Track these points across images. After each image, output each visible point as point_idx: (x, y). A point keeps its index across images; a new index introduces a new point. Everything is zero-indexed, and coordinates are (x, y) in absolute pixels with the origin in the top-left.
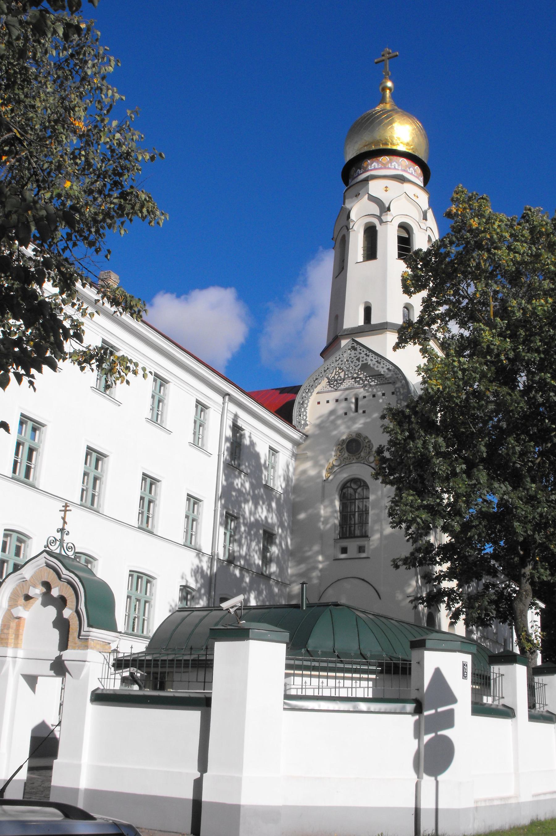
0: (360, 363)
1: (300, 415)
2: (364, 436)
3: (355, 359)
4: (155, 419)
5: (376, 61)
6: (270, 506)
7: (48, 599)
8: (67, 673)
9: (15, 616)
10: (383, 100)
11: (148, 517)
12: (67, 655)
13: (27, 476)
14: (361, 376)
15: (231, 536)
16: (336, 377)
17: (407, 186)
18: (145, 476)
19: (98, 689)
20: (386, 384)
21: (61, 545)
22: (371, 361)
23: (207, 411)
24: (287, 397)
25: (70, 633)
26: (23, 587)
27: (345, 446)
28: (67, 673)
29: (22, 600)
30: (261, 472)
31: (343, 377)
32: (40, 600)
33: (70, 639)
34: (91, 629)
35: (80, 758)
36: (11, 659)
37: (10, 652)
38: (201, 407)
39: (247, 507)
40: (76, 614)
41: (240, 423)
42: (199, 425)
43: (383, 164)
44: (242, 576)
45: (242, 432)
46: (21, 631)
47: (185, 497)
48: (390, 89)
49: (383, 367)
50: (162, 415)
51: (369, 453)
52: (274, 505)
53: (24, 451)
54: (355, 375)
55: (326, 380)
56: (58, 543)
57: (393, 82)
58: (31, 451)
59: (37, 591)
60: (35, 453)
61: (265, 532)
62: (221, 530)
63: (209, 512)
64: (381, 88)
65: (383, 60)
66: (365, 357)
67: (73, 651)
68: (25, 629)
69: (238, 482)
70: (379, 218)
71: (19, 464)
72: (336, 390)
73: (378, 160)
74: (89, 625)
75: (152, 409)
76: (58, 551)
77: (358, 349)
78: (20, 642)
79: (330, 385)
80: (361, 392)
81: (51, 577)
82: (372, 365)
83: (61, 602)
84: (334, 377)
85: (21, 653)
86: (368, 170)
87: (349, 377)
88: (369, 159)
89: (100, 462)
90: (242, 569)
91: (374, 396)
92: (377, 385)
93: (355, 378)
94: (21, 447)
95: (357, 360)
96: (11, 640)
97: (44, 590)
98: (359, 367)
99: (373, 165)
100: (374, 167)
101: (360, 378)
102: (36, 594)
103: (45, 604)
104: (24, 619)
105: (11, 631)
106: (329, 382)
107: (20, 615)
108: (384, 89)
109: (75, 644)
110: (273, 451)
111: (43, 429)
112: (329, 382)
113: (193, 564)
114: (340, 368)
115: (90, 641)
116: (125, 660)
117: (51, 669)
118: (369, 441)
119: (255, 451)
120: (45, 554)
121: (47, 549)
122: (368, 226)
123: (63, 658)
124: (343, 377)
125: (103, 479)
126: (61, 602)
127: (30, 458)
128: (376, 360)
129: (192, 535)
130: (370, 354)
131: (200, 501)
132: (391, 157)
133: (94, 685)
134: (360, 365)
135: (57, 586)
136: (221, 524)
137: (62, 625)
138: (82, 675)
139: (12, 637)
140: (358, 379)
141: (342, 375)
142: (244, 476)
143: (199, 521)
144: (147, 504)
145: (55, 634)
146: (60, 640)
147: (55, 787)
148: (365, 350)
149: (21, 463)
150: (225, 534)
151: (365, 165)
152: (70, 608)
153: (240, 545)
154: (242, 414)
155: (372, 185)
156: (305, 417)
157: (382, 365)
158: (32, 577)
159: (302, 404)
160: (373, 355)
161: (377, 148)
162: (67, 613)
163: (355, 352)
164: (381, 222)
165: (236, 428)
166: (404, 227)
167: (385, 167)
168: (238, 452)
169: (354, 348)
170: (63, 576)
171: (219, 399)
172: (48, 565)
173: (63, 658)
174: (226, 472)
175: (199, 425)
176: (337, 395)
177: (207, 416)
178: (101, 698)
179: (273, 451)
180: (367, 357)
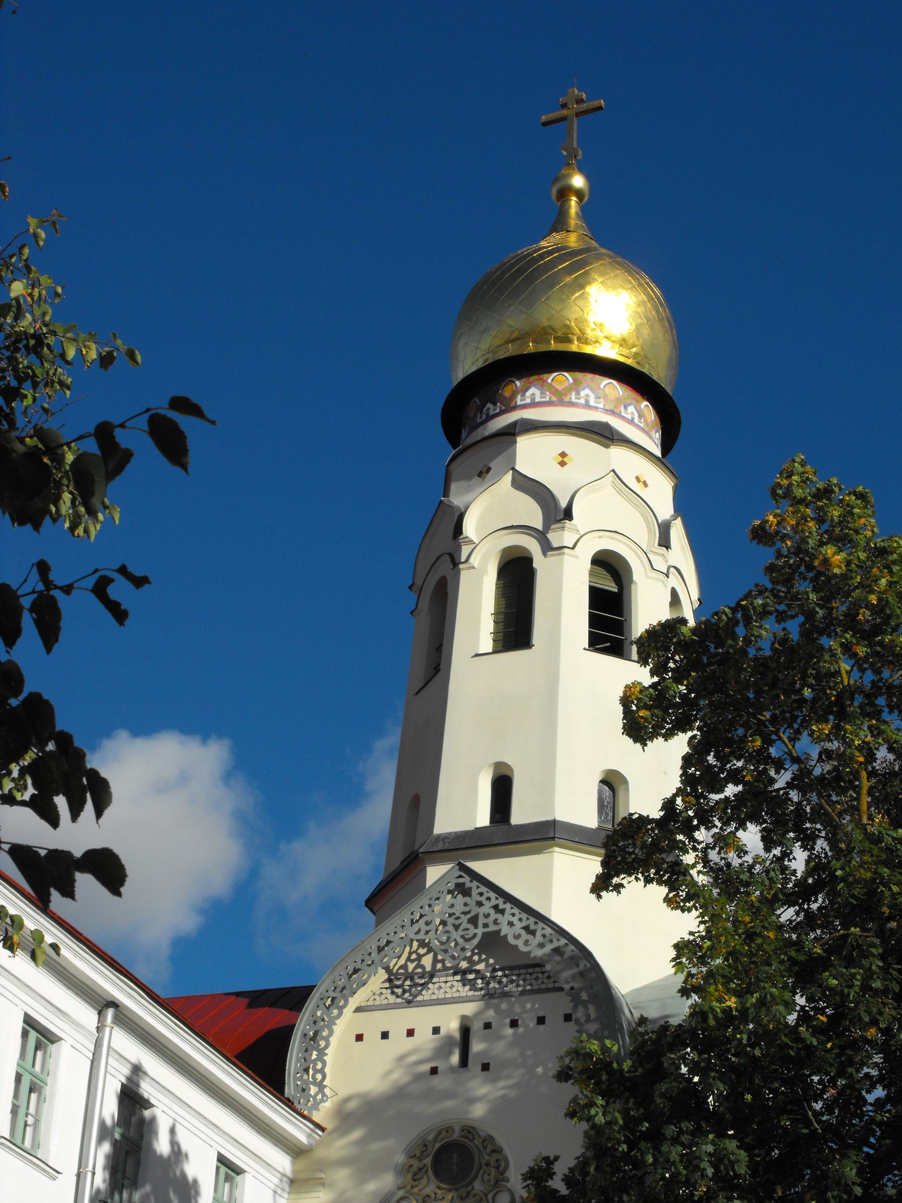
0: (480, 931)
1: (306, 1070)
3: (464, 919)
5: (544, 118)
10: (559, 223)
14: (481, 967)
16: (411, 967)
17: (618, 455)
22: (511, 927)
23: (52, 1048)
24: (269, 1019)
27: (428, 1161)
31: (428, 968)
38: (37, 1036)
41: (146, 1089)
43: (555, 392)
48: (579, 194)
51: (497, 1182)
55: (382, 975)
64: (554, 190)
65: (564, 119)
66: (493, 915)
70: (541, 536)
73: (545, 381)
77: (475, 892)
79: (392, 987)
84: (405, 967)
87: (445, 968)
92: (523, 993)
93: (464, 972)
98: (475, 942)
99: (528, 394)
100: (533, 399)
101: (478, 972)
108: (565, 192)
112: (389, 980)
118: (498, 1150)
124: (428, 968)
128: (524, 924)
130: (508, 906)
132: (579, 375)
140: (471, 976)
141: (427, 961)
148: (492, 895)
151: (507, 392)
155: (525, 444)
156: (319, 1077)
159: (314, 1039)
160: (516, 911)
161: (543, 348)
163: (467, 899)
164: (547, 547)
165: (131, 1099)
166: (608, 564)
167: (560, 400)
171: (88, 1016)
177: (51, 1063)
180: (499, 916)
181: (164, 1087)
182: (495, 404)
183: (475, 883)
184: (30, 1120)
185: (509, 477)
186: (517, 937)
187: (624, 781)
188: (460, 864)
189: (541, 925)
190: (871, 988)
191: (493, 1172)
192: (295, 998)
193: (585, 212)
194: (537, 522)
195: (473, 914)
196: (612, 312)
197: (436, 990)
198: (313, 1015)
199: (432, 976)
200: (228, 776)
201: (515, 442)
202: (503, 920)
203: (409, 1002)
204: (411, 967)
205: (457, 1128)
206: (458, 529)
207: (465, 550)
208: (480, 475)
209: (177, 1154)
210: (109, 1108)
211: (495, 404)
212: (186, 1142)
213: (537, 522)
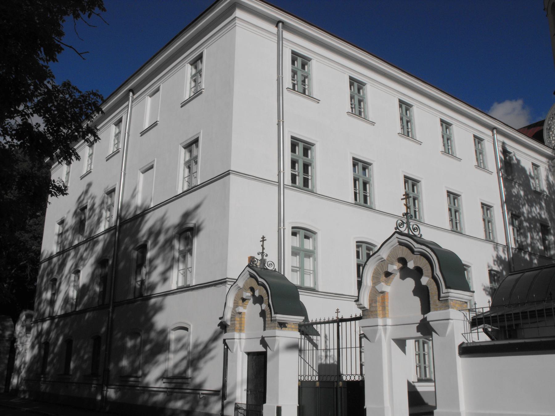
1: (550, 138)
4: (447, 152)
6: (541, 204)
7: (405, 272)
8: (433, 333)
9: (380, 291)
11: (456, 223)
12: (430, 316)
13: (365, 201)
15: (518, 231)
18: (449, 193)
19: (463, 343)
21: (408, 227)
23: (482, 142)
24: (537, 129)
25: (431, 297)
26: (382, 266)
28: (433, 333)
29: (383, 277)
30: (529, 181)
32: (398, 275)
33: (431, 302)
34: (450, 290)
35: (458, 406)
37: (380, 321)
38: (478, 140)
39: (525, 209)
40: (432, 280)
41: (509, 149)
42: (479, 153)
44: (531, 260)
45: (511, 155)
46: (386, 303)
47: (480, 205)
50: (451, 149)
52: (543, 204)
53: (360, 185)
56: (405, 225)
58: (365, 184)
59: (395, 267)
60: (368, 185)
61: (542, 225)
62: (510, 229)
63: (499, 215)
67: (436, 312)
68: (389, 301)
69: (515, 191)
71: (358, 195)
74: (447, 287)
75: (444, 145)
76: (406, 232)
78: (387, 312)
81: (404, 252)
83: (418, 273)
85: (389, 321)
89: (415, 187)
90: (530, 254)
94: (357, 182)
96: (380, 312)
97: (401, 265)
102: (394, 270)
103: (403, 277)
104: (388, 293)
105: (378, 304)
107: (384, 290)
109: (437, 305)
110: (535, 166)
111: (370, 167)
113: (493, 257)
115: (450, 302)
116: (478, 319)
117: (418, 331)
119: (522, 167)
120: (396, 235)
121: (398, 230)
125: (420, 198)
126: (418, 273)
127: (365, 189)
129: (489, 233)
131: (491, 207)
133: (459, 340)
135: (412, 259)
136: (509, 224)
137: (421, 292)
138: (448, 333)
139: (379, 309)
142: (519, 186)
143: (493, 221)
144: (454, 213)
145: (417, 301)
146: (421, 305)
149: (359, 193)
150: (513, 229)
152: (427, 276)
153: (526, 237)
154: (507, 141)
158: (389, 256)
159: (550, 129)
162: (425, 280)
165: (505, 152)
168: (510, 169)
170: (416, 250)
171: (489, 133)
172: (401, 244)
173: (428, 320)
174: (507, 184)
175: (479, 153)
177: (483, 146)
178: (467, 350)
179: (535, 166)
181: (511, 146)
184: (482, 161)
190: (544, 247)
192: (542, 123)
198: (548, 123)
200: (523, 108)
209: (518, 161)
210: (500, 155)
212: (519, 158)
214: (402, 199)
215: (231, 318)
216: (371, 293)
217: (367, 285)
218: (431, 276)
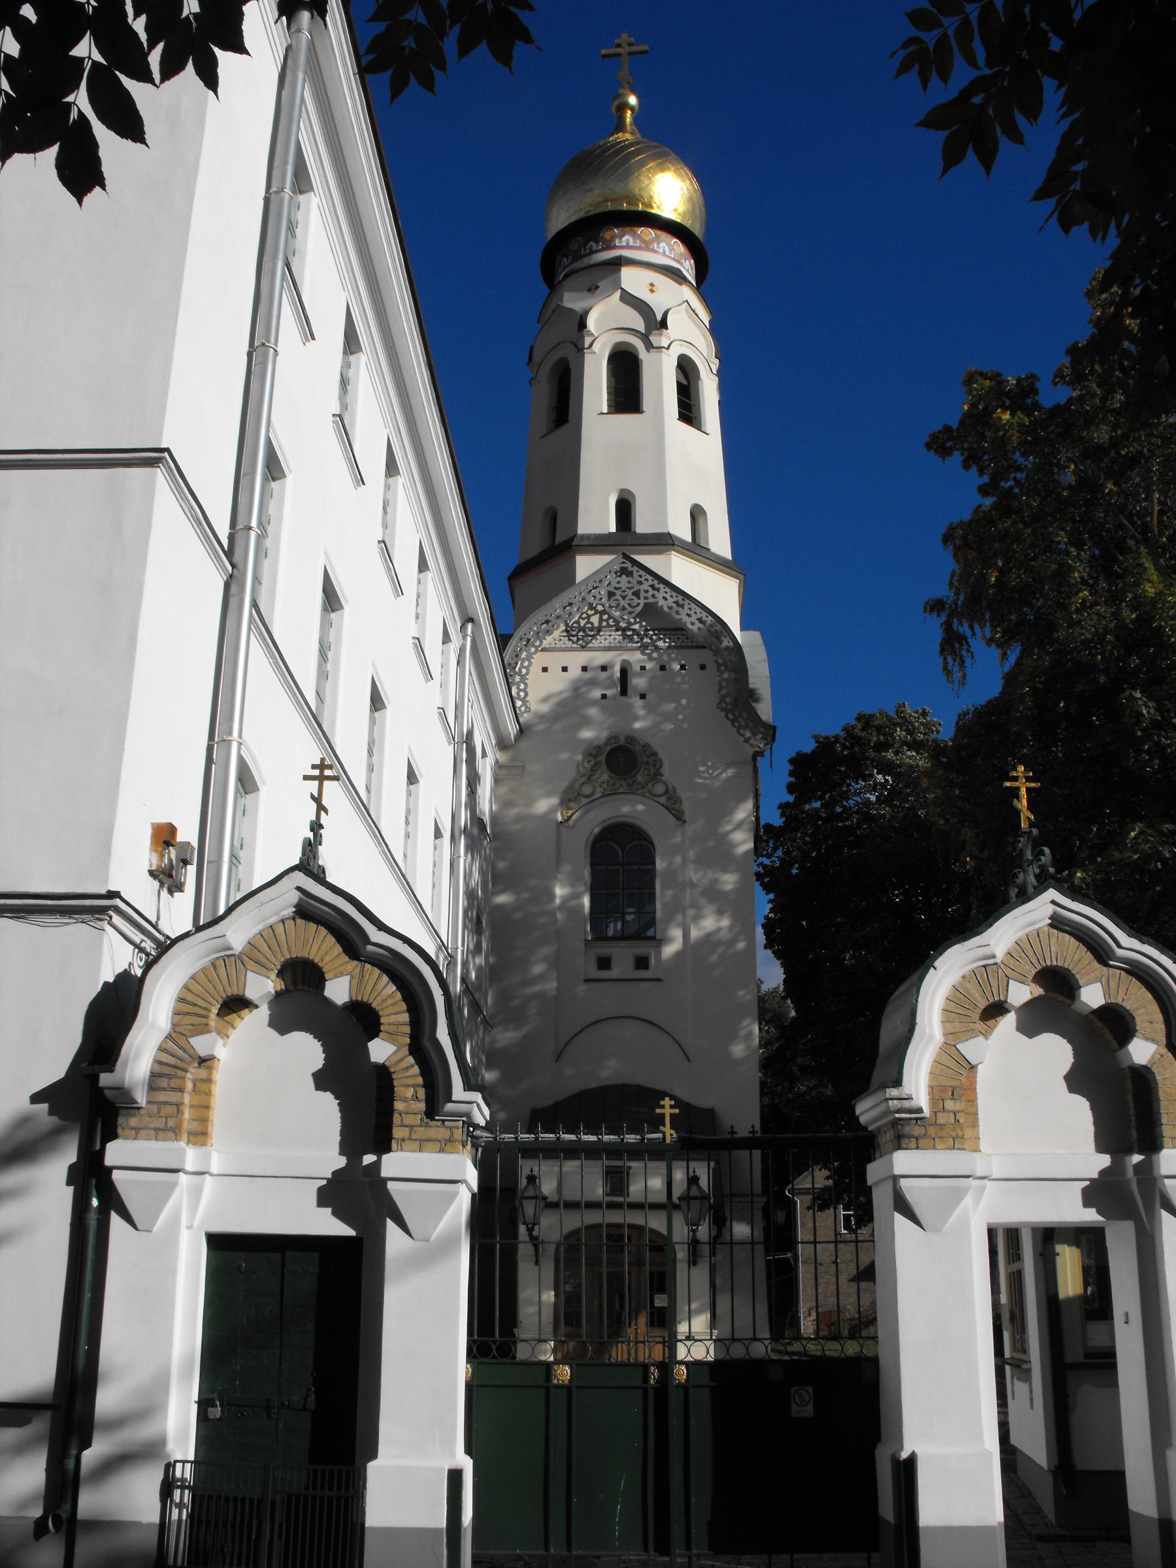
0: (642, 602)
2: (642, 743)
3: (629, 592)
5: (603, 52)
10: (620, 127)
14: (636, 627)
16: (582, 623)
20: (687, 647)
22: (665, 600)
27: (602, 758)
31: (596, 625)
36: (214, 1169)
43: (644, 241)
48: (632, 109)
49: (689, 615)
51: (655, 775)
54: (623, 625)
55: (563, 627)
57: (639, 98)
59: (261, 986)
64: (616, 103)
65: (619, 55)
66: (651, 592)
72: (583, 647)
73: (635, 233)
77: (635, 574)
79: (569, 636)
80: (636, 658)
81: (1068, 953)
82: (666, 609)
84: (578, 622)
86: (615, 247)
87: (609, 626)
88: (616, 227)
91: (663, 668)
92: (669, 647)
93: (624, 630)
95: (634, 594)
98: (640, 608)
99: (624, 239)
100: (627, 243)
101: (634, 630)
106: (567, 631)
108: (625, 106)
112: (567, 631)
114: (591, 607)
117: (1087, 1203)
118: (654, 754)
122: (626, 349)
123: (384, 1174)
124: (596, 625)
128: (675, 599)
130: (661, 586)
132: (658, 232)
134: (642, 605)
140: (629, 633)
141: (595, 620)
146: (1095, 1123)
147: (929, 1528)
148: (650, 578)
151: (607, 235)
155: (626, 273)
156: (522, 694)
157: (686, 610)
160: (668, 590)
161: (633, 208)
163: (630, 579)
164: (649, 346)
169: (623, 571)
176: (582, 658)
180: (656, 592)
182: (597, 243)
183: (635, 568)
185: (618, 294)
186: (670, 608)
187: (704, 513)
188: (624, 554)
189: (687, 601)
191: (652, 769)
193: (635, 120)
194: (641, 328)
195: (636, 589)
196: (670, 191)
197: (600, 641)
199: (599, 630)
201: (620, 270)
202: (660, 595)
203: (583, 647)
204: (582, 623)
205: (622, 738)
206: (582, 325)
207: (587, 341)
208: (590, 290)
211: (597, 243)
213: (641, 328)
214: (306, 778)
215: (154, 1075)
216: (937, 1062)
217: (932, 1036)
218: (1164, 1041)
